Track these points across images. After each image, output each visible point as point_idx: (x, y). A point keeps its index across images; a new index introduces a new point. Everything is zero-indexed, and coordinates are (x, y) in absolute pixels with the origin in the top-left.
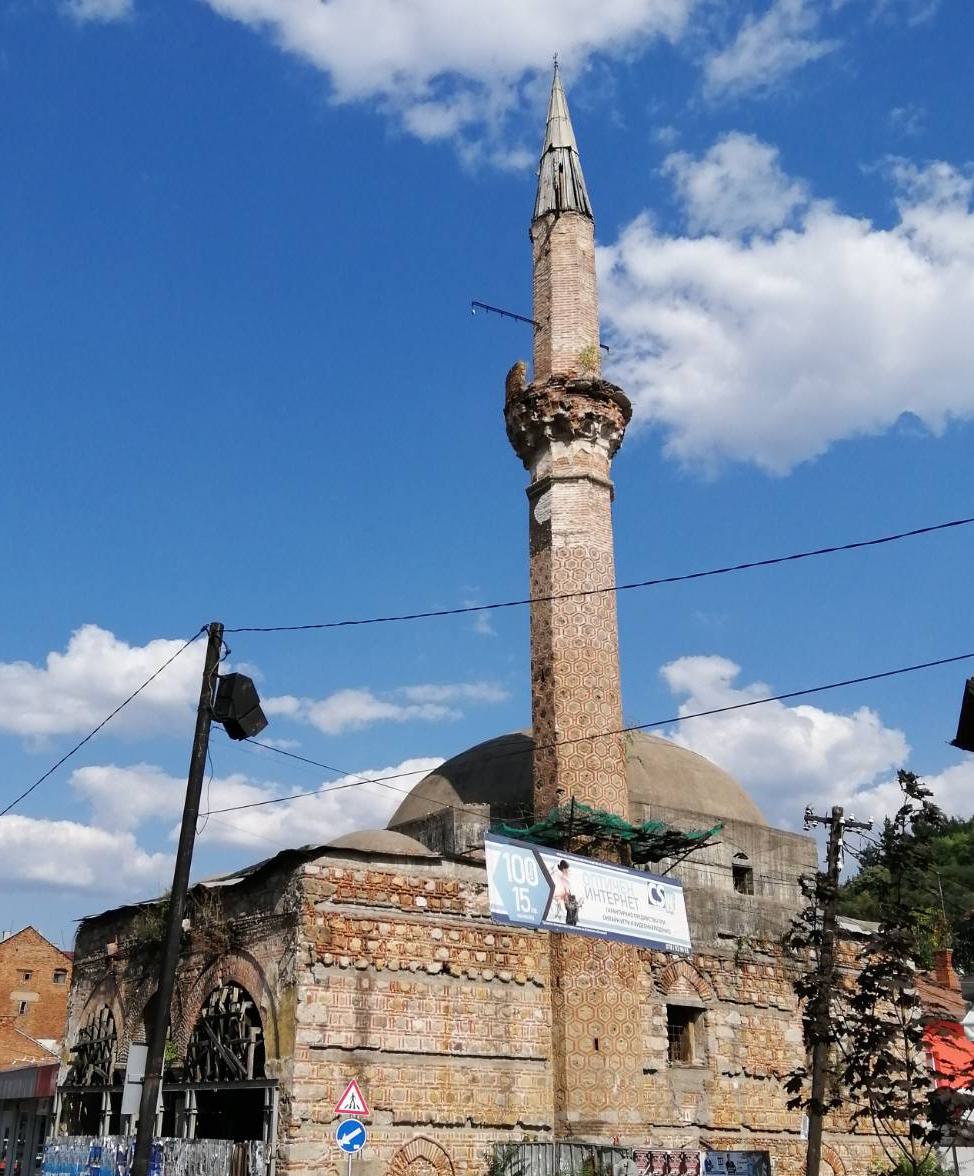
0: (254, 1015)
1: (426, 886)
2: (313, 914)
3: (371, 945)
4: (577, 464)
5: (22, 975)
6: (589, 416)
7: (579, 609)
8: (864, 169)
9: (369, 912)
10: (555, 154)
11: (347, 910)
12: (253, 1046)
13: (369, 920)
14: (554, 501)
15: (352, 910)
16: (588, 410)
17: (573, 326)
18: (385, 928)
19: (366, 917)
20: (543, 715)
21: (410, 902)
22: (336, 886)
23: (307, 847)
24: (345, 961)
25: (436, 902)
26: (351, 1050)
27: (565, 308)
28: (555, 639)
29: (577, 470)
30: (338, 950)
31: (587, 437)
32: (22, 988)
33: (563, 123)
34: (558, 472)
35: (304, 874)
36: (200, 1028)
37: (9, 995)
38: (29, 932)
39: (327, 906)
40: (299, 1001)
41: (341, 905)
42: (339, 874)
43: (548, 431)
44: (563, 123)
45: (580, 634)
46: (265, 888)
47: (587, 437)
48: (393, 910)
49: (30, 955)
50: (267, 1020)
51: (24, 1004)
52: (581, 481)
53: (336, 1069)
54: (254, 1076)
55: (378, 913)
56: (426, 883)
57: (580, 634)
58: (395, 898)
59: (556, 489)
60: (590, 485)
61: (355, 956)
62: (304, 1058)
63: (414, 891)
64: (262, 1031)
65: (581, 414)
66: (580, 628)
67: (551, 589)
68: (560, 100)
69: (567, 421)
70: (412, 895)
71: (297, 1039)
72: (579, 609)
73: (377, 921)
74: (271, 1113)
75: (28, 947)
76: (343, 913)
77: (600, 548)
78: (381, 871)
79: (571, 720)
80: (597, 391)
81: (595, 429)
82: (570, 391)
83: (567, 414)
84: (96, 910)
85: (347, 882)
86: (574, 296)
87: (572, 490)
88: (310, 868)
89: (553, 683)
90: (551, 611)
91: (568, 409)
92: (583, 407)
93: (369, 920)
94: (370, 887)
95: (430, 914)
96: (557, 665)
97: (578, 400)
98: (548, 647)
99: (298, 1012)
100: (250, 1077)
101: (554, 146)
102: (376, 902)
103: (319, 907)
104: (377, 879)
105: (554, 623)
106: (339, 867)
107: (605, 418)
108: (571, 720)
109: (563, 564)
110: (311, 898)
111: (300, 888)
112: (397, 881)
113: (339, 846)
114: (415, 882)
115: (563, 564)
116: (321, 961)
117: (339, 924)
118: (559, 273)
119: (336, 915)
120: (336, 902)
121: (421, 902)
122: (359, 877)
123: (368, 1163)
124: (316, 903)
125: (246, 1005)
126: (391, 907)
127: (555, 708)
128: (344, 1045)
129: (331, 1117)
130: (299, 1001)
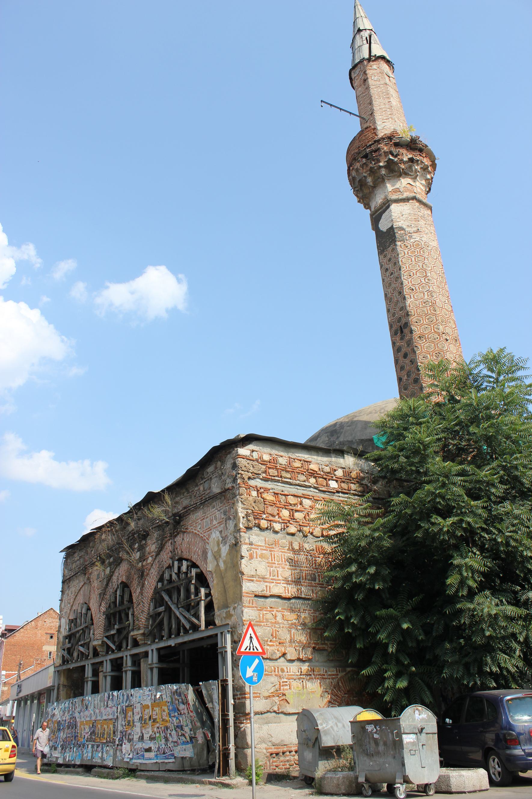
0: (202, 580)
1: (336, 473)
2: (249, 487)
3: (297, 515)
4: (406, 191)
5: (49, 636)
6: (411, 160)
7: (423, 281)
9: (293, 490)
10: (362, 33)
11: (276, 487)
12: (203, 604)
13: (294, 496)
15: (279, 487)
16: (410, 156)
18: (307, 503)
19: (291, 493)
20: (405, 356)
21: (325, 484)
22: (264, 467)
23: (238, 436)
24: (277, 527)
25: (344, 486)
26: (289, 599)
28: (408, 302)
30: (271, 518)
31: (411, 175)
32: (49, 644)
33: (365, 20)
34: (394, 197)
35: (239, 456)
36: (158, 600)
37: (42, 648)
38: (52, 612)
39: (258, 483)
40: (242, 557)
41: (270, 483)
42: (266, 457)
43: (383, 172)
44: (365, 20)
45: (426, 297)
46: (202, 479)
47: (411, 175)
48: (312, 489)
49: (52, 624)
50: (213, 582)
51: (50, 653)
53: (279, 615)
54: (206, 626)
55: (300, 491)
56: (335, 470)
57: (426, 297)
58: (312, 480)
59: (394, 207)
60: (417, 204)
61: (286, 524)
62: (251, 605)
63: (329, 476)
64: (210, 590)
65: (405, 159)
66: (426, 293)
67: (400, 270)
68: (361, 10)
69: (396, 163)
70: (325, 479)
71: (243, 589)
72: (423, 281)
73: (300, 497)
74: (226, 652)
75: (51, 620)
76: (272, 489)
77: (431, 244)
78: (299, 458)
79: (428, 356)
80: (413, 145)
82: (397, 145)
83: (396, 159)
84: (74, 539)
85: (273, 463)
86: (387, 101)
88: (243, 451)
89: (411, 332)
90: (402, 284)
92: (406, 155)
93: (294, 496)
94: (289, 468)
95: (340, 494)
96: (413, 319)
98: (404, 308)
99: (243, 566)
100: (203, 627)
102: (298, 482)
103: (252, 483)
104: (297, 464)
105: (406, 291)
106: (266, 453)
107: (422, 162)
108: (428, 356)
109: (406, 253)
110: (246, 475)
111: (235, 466)
112: (313, 467)
113: (191, 794)
114: (327, 469)
115: (406, 253)
116: (259, 526)
117: (269, 497)
118: (375, 89)
119: (267, 490)
120: (266, 480)
121: (333, 484)
122: (283, 461)
124: (249, 478)
125: (194, 571)
126: (310, 487)
127: (415, 349)
128: (283, 595)
129: (279, 654)
130: (242, 557)
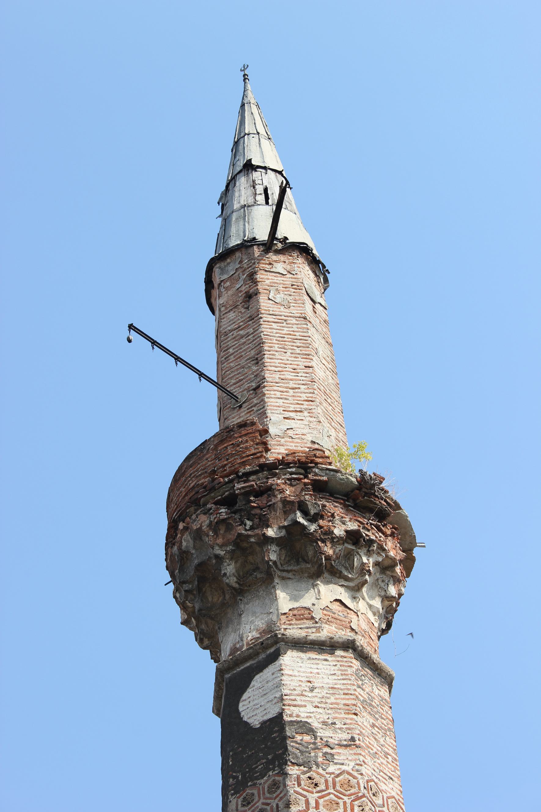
6: (353, 537)
8: (391, 788)
10: (256, 175)
14: (286, 680)
16: (353, 526)
17: (306, 405)
27: (289, 376)
29: (327, 632)
31: (347, 579)
34: (294, 631)
52: (339, 653)
59: (290, 659)
65: (339, 531)
69: (312, 539)
81: (363, 564)
82: (320, 488)
87: (322, 665)
91: (313, 519)
97: (335, 508)
101: (253, 162)
123: (202, 540)
